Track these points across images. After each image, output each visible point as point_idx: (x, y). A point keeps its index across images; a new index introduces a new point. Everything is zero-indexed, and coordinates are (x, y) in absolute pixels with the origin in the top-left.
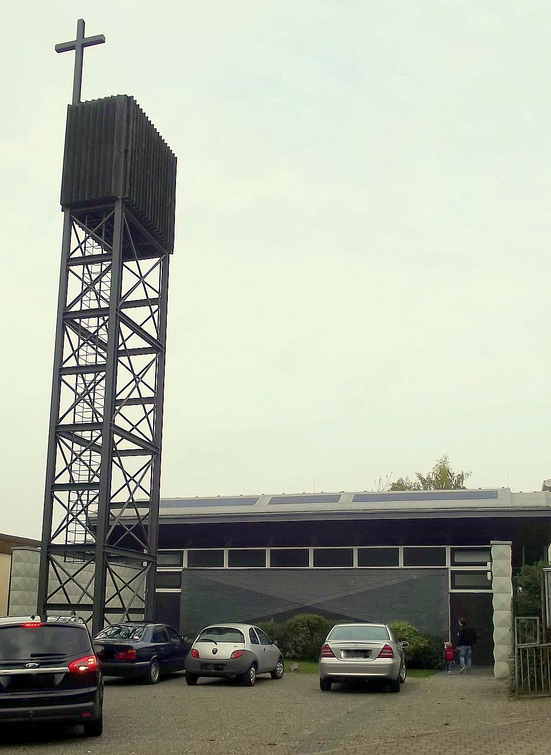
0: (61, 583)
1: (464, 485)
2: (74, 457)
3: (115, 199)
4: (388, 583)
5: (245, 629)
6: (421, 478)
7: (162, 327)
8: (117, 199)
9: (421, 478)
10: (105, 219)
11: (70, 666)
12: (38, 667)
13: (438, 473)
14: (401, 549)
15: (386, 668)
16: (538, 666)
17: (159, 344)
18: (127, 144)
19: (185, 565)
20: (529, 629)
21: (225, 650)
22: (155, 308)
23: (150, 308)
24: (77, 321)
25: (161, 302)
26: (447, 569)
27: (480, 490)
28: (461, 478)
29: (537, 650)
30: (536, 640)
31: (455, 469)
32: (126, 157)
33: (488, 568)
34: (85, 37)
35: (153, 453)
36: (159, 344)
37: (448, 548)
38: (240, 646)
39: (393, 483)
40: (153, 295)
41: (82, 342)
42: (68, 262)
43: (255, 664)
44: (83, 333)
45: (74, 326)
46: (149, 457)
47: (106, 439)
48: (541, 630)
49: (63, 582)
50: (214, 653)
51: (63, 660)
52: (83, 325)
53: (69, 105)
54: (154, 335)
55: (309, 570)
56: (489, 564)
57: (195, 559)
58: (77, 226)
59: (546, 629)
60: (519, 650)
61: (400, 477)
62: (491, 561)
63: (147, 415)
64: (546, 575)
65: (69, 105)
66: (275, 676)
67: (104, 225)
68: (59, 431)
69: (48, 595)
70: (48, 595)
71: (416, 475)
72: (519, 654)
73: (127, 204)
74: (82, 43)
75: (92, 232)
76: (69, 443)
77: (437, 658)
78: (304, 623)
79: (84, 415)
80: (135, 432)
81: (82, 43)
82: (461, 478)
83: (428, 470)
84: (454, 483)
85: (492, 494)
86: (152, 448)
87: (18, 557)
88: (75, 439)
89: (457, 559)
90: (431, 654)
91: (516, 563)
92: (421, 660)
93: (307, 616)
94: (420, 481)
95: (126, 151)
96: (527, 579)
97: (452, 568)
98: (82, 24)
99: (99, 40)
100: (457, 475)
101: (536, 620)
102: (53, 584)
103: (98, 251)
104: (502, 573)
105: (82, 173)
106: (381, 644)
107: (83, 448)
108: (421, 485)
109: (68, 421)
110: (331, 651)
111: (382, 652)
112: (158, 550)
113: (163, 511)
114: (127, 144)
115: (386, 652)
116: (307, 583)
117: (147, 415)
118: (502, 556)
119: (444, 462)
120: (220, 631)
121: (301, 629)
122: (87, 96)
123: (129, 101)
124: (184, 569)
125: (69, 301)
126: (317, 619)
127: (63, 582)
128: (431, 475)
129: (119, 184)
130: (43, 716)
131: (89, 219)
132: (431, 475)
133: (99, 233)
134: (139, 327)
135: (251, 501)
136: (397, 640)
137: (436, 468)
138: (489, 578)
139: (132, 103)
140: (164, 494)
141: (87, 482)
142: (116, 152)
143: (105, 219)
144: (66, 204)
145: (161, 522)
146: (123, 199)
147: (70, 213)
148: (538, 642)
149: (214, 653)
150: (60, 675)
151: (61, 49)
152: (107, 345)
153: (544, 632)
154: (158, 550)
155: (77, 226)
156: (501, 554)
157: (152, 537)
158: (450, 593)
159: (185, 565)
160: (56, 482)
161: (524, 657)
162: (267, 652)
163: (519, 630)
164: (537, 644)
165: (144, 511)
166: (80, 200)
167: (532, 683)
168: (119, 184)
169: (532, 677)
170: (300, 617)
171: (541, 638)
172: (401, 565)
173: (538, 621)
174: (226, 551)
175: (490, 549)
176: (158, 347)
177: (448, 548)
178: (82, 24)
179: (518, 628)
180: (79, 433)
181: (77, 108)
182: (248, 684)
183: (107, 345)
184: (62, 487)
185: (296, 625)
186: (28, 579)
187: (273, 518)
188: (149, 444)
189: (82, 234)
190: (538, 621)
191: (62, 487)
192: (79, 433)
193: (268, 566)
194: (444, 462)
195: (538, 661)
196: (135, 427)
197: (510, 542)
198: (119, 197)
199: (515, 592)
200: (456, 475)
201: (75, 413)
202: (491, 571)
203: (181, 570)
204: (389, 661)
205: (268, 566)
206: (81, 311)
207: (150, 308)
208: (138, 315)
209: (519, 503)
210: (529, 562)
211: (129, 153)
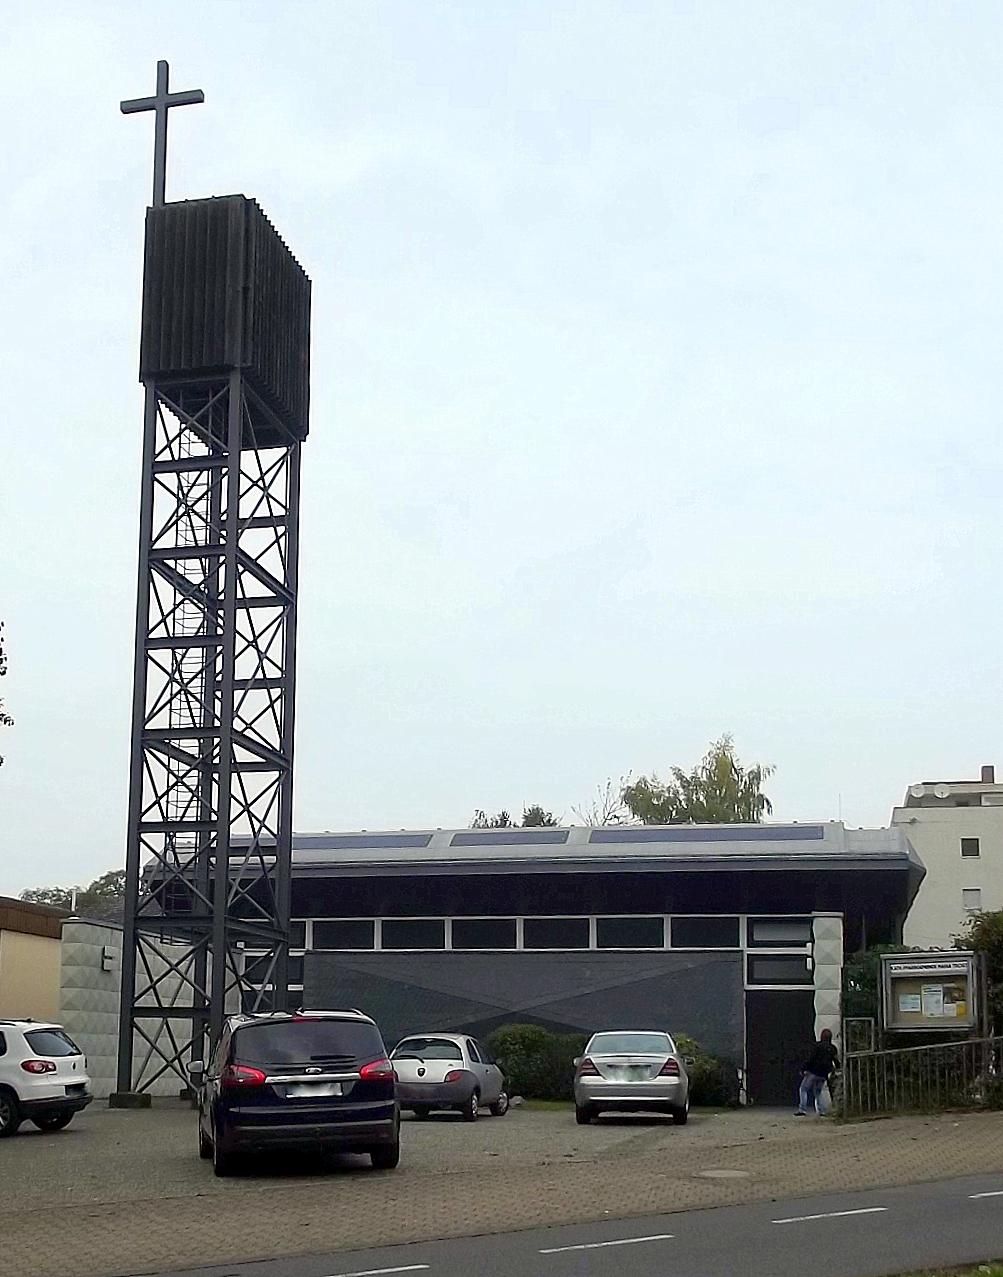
0: (151, 980)
1: (761, 792)
2: (173, 780)
3: (230, 369)
4: (646, 975)
5: (460, 1041)
6: (681, 777)
7: (291, 562)
8: (233, 368)
9: (681, 777)
10: (212, 401)
11: (362, 1072)
12: (322, 1073)
13: (713, 768)
14: (667, 918)
15: (670, 1090)
16: (872, 1080)
17: (289, 592)
18: (247, 276)
19: (309, 945)
20: (862, 1034)
21: (438, 1070)
22: (281, 530)
23: (275, 530)
24: (171, 563)
25: (288, 522)
26: (742, 951)
27: (795, 825)
28: (756, 777)
29: (871, 1059)
30: (870, 1048)
31: (745, 760)
32: (245, 298)
33: (807, 950)
34: (170, 92)
35: (280, 769)
36: (289, 592)
37: (743, 919)
38: (457, 1065)
39: (629, 787)
40: (279, 511)
41: (180, 598)
42: (153, 468)
43: (477, 1090)
44: (179, 582)
45: (167, 571)
46: (275, 774)
47: (215, 749)
48: (877, 1035)
49: (155, 979)
50: (421, 1074)
51: (354, 1063)
52: (180, 570)
53: (148, 208)
54: (279, 574)
55: (515, 953)
56: (809, 945)
57: (323, 936)
58: (162, 406)
59: (884, 1034)
60: (848, 1060)
61: (641, 775)
62: (813, 942)
63: (272, 703)
64: (883, 962)
65: (148, 208)
66: (496, 1110)
67: (211, 409)
68: (146, 741)
69: (136, 996)
70: (136, 996)
71: (671, 772)
72: (848, 1065)
73: (248, 375)
74: (163, 102)
75: (192, 420)
76: (164, 758)
77: (727, 1089)
78: (514, 1038)
79: (181, 716)
80: (249, 733)
81: (163, 102)
82: (756, 777)
83: (695, 762)
84: (742, 787)
85: (814, 832)
86: (279, 760)
87: (72, 935)
88: (172, 752)
89: (757, 938)
90: (718, 1083)
91: (851, 945)
92: (711, 1091)
93: (519, 1026)
94: (678, 783)
95: (246, 289)
96: (860, 968)
97: (743, 944)
98: (163, 68)
99: (195, 98)
100: (747, 772)
101: (870, 1022)
102: (142, 980)
103: (201, 450)
104: (829, 960)
105: (174, 324)
106: (664, 1058)
107: (188, 768)
108: (681, 790)
109: (159, 722)
110: (595, 1068)
111: (664, 1068)
112: (292, 920)
113: (297, 856)
114: (247, 276)
115: (668, 1069)
116: (522, 973)
117: (272, 703)
118: (828, 934)
119: (724, 748)
120: (420, 1044)
121: (512, 1047)
122: (177, 192)
123: (250, 206)
124: (308, 953)
125: (158, 526)
126: (535, 1032)
127: (155, 979)
128: (699, 772)
129: (225, 325)
130: (297, 1137)
131: (185, 398)
132: (699, 772)
133: (203, 421)
134: (254, 562)
135: (422, 839)
136: (681, 1055)
137: (709, 759)
138: (809, 967)
139: (254, 207)
140: (299, 828)
141: (194, 819)
142: (229, 292)
143: (212, 401)
144: (149, 374)
145: (296, 875)
146: (242, 369)
147: (156, 387)
148: (873, 1050)
149: (421, 1074)
150: (349, 1083)
151: (129, 108)
152: (215, 592)
153: (880, 1036)
154: (292, 920)
155: (162, 406)
156: (828, 933)
157: (282, 898)
158: (747, 991)
159: (309, 945)
160: (144, 819)
161: (855, 1068)
162: (487, 1073)
163: (850, 1035)
164: (871, 1052)
165: (270, 859)
166: (172, 367)
167: (865, 1102)
168: (225, 325)
169: (865, 1094)
170: (506, 1029)
171: (876, 1044)
172: (667, 946)
173: (873, 1022)
174: (378, 922)
175: (810, 921)
176: (285, 595)
177: (743, 919)
178: (163, 68)
179: (847, 1033)
180: (175, 743)
181: (163, 214)
182: (468, 1117)
183: (215, 592)
184: (153, 827)
185: (504, 1042)
186: (87, 970)
187: (473, 868)
188: (273, 751)
189: (173, 423)
190: (873, 1022)
191: (153, 827)
192: (175, 743)
193: (448, 947)
194: (724, 748)
195: (872, 1074)
196: (249, 726)
197: (841, 914)
198: (236, 366)
199: (845, 987)
200: (746, 771)
201: (171, 710)
202: (812, 957)
203: (302, 954)
204: (674, 1080)
205: (448, 947)
206: (177, 548)
207: (275, 530)
208: (253, 542)
209: (857, 848)
210: (872, 941)
211: (251, 294)
